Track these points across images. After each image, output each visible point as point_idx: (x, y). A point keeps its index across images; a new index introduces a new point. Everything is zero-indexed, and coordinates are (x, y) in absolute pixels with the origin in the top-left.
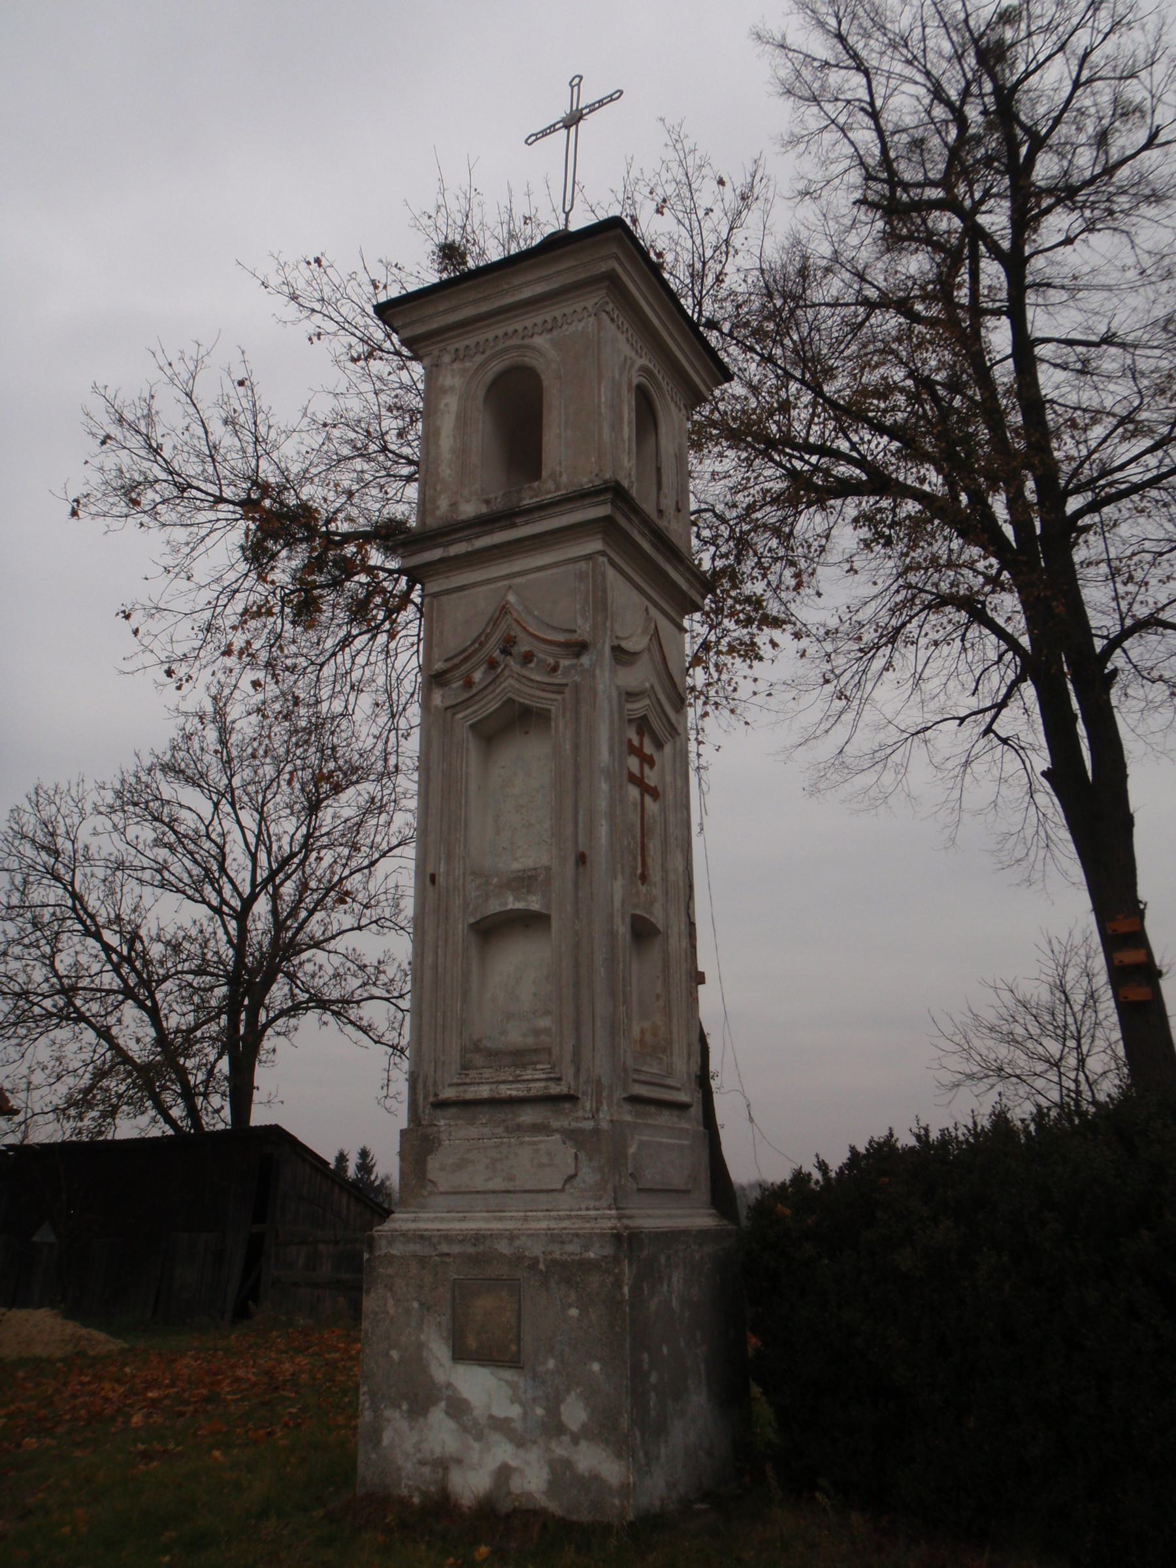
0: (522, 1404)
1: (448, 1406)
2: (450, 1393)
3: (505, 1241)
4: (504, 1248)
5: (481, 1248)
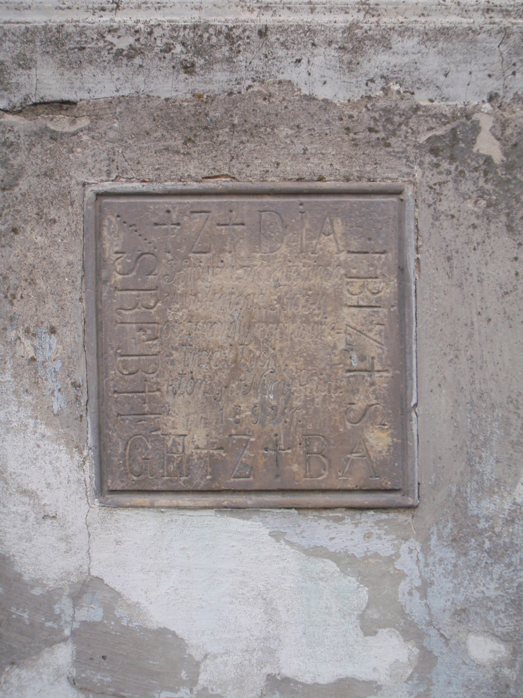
0: (411, 632)
1: (79, 660)
2: (91, 612)
3: (323, 58)
4: (321, 78)
5: (218, 81)
